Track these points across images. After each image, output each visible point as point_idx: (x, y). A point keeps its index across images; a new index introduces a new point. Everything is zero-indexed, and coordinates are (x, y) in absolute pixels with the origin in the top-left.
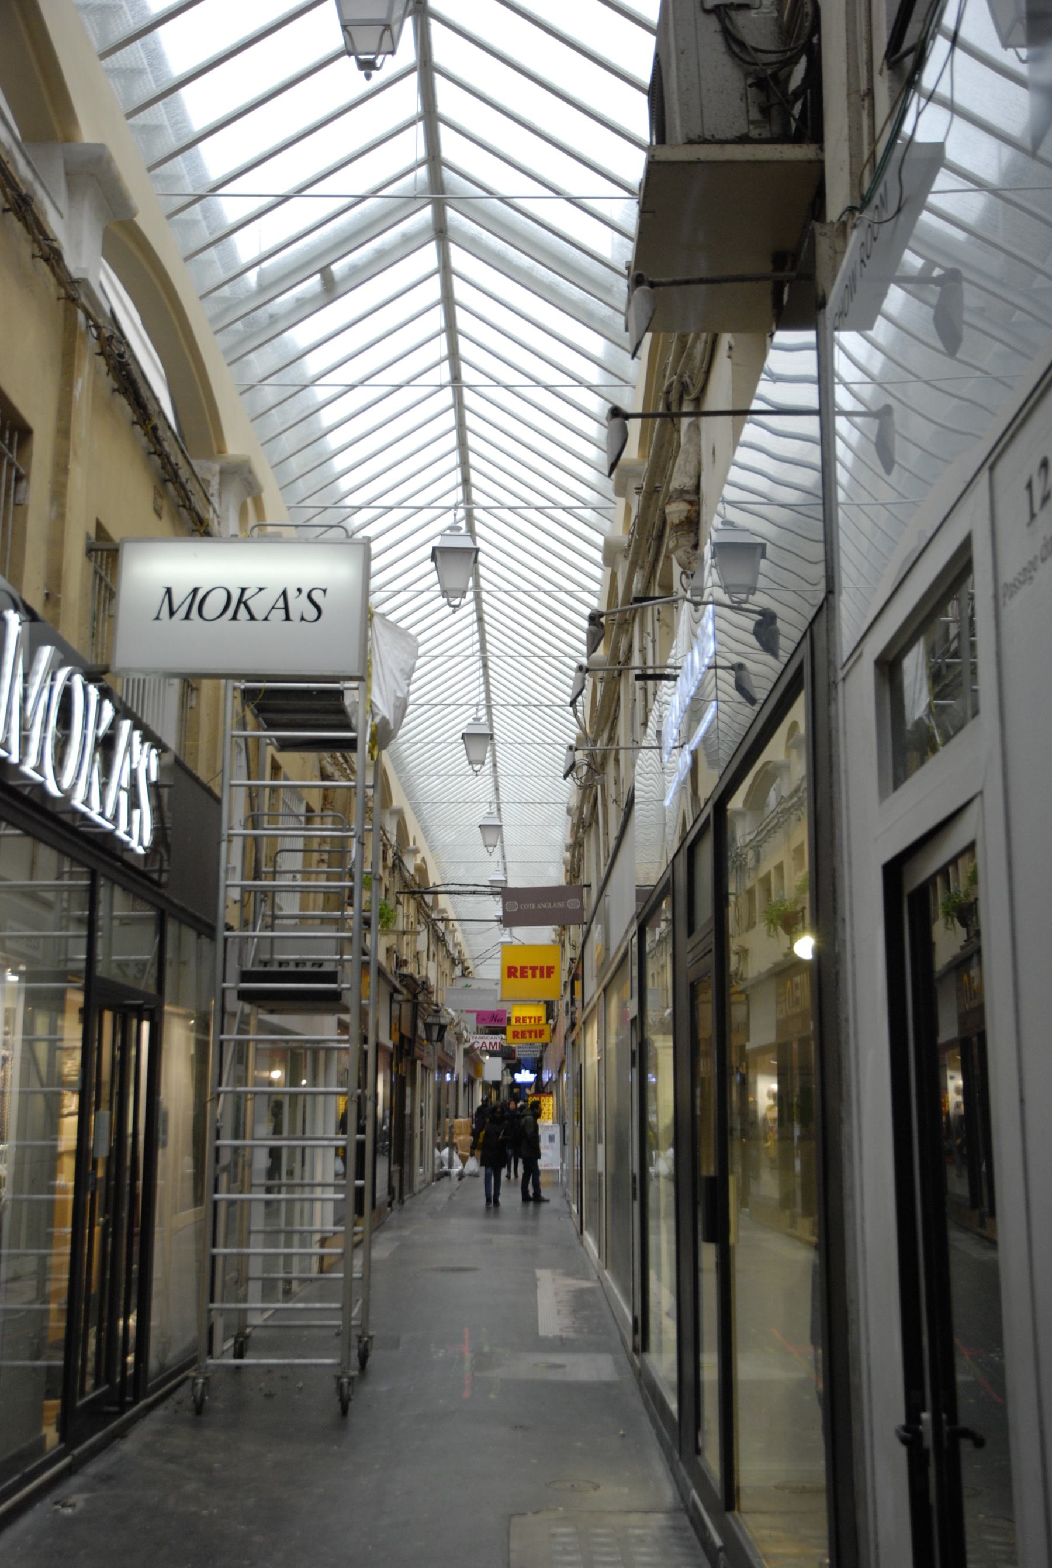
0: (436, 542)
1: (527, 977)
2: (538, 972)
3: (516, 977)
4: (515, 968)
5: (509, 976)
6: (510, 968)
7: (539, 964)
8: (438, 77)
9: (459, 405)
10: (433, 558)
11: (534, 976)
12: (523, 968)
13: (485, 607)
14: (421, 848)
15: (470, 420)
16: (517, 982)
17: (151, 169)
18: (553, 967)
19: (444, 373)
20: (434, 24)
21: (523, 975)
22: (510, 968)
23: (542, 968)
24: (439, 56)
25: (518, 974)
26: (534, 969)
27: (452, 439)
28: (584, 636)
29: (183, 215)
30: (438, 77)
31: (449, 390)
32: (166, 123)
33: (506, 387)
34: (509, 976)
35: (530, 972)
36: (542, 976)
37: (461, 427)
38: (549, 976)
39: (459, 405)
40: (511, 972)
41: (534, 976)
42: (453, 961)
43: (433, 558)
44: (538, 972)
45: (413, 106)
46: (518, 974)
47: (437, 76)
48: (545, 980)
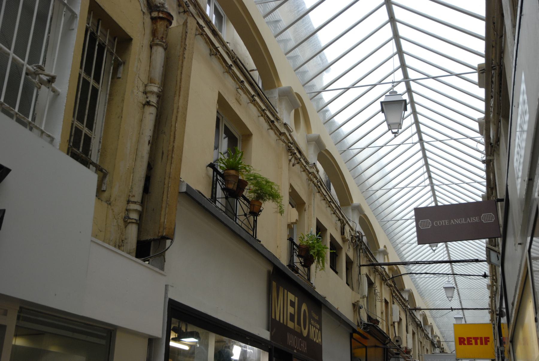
0: (383, 99)
1: (472, 344)
2: (479, 341)
3: (465, 344)
4: (463, 338)
5: (460, 344)
6: (460, 339)
7: (479, 336)
8: (405, 55)
9: (423, 149)
10: (383, 111)
11: (476, 344)
12: (469, 339)
13: (437, 193)
14: (461, 346)
15: (428, 154)
16: (466, 348)
17: (295, 71)
18: (488, 338)
19: (416, 138)
20: (398, 24)
21: (469, 343)
22: (460, 339)
23: (481, 338)
24: (401, 33)
25: (466, 342)
26: (476, 339)
27: (420, 154)
28: (485, 252)
29: (301, 69)
30: (401, 40)
31: (419, 144)
32: (299, 54)
33: (440, 141)
34: (460, 344)
35: (473, 341)
36: (482, 344)
37: (425, 157)
38: (486, 344)
39: (423, 149)
40: (461, 341)
41: (476, 344)
42: (433, 344)
43: (383, 111)
44: (479, 341)
45: (398, 63)
46: (466, 342)
47: (408, 69)
48: (484, 346)
